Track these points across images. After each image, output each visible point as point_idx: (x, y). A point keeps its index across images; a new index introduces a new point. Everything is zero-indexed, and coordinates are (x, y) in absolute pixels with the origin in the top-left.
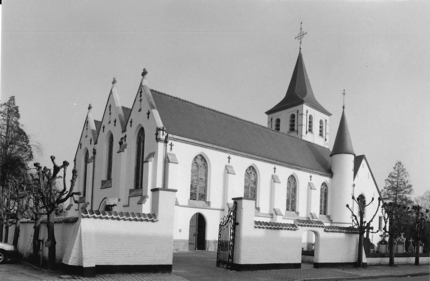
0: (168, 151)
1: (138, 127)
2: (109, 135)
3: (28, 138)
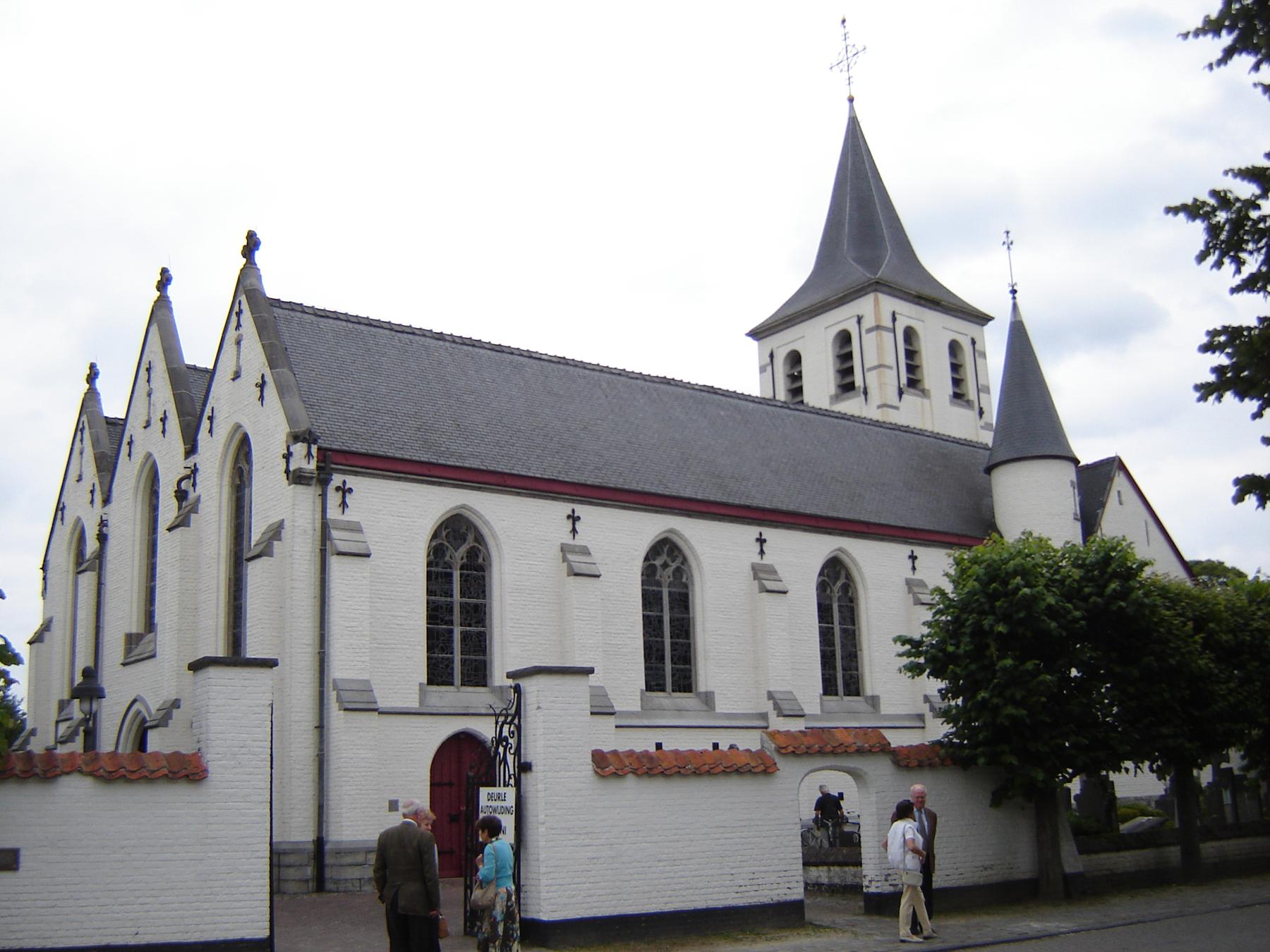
0: (333, 513)
2: (145, 475)
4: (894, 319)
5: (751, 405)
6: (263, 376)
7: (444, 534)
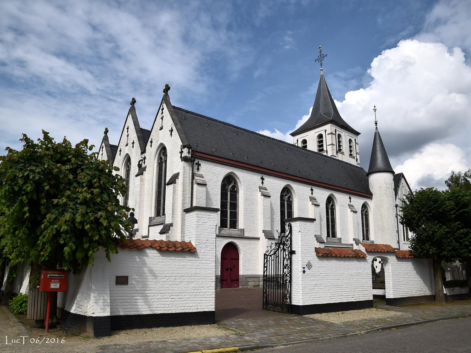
0: (196, 171)
1: (158, 150)
3: (19, 147)
4: (336, 132)
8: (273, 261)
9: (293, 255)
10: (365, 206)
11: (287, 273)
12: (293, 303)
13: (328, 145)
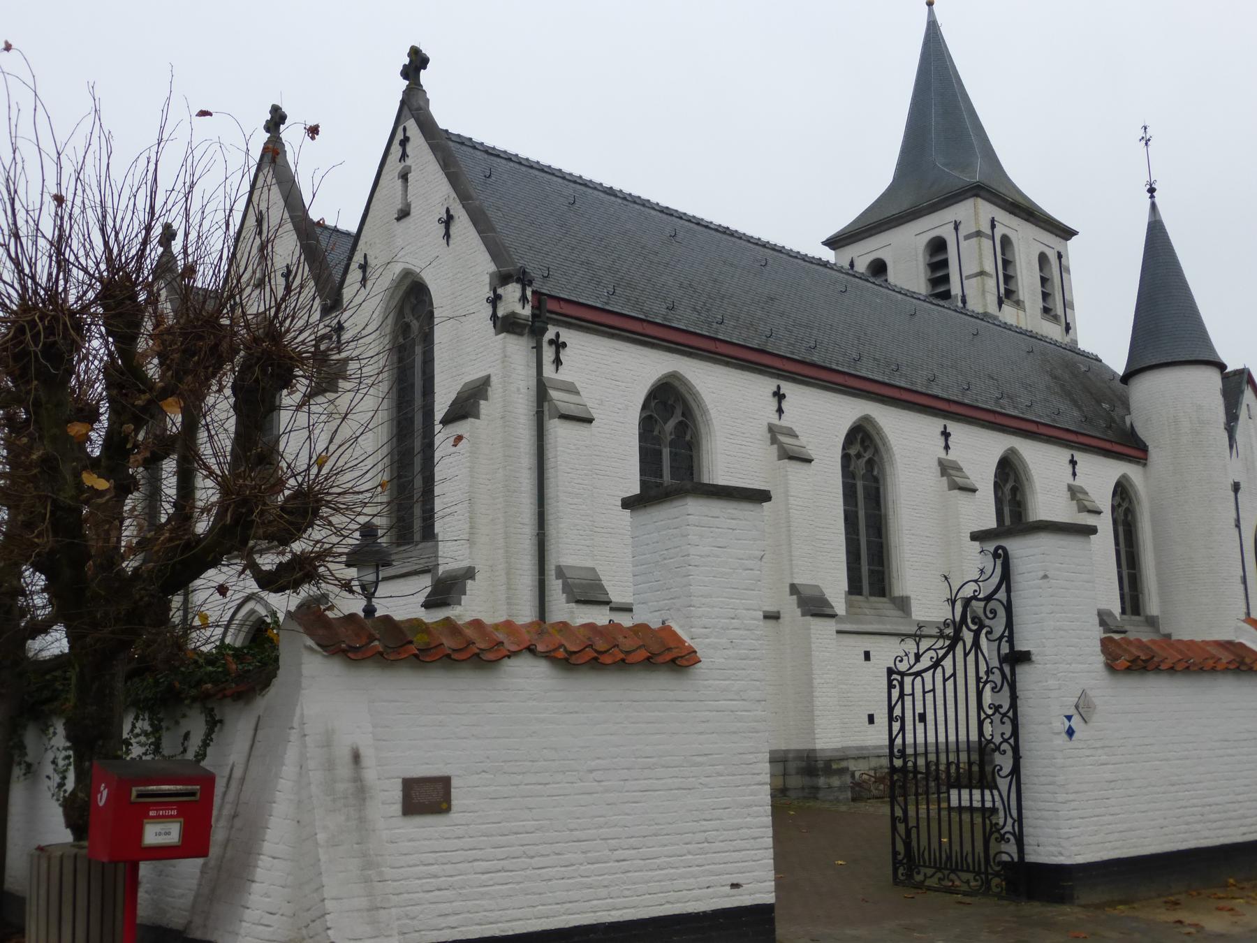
0: (549, 370)
4: (993, 227)
5: (900, 296)
6: (448, 211)
7: (653, 404)
8: (929, 696)
9: (1023, 672)
10: (1122, 491)
11: (998, 740)
12: (1031, 858)
13: (968, 277)
